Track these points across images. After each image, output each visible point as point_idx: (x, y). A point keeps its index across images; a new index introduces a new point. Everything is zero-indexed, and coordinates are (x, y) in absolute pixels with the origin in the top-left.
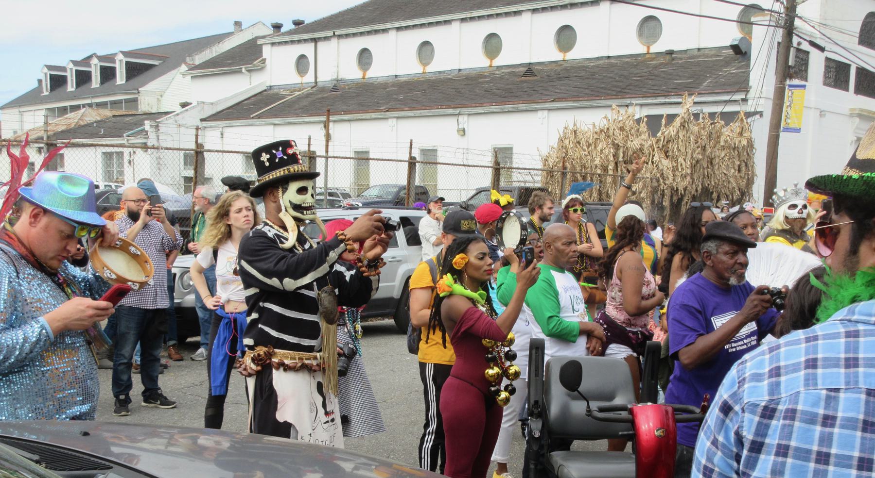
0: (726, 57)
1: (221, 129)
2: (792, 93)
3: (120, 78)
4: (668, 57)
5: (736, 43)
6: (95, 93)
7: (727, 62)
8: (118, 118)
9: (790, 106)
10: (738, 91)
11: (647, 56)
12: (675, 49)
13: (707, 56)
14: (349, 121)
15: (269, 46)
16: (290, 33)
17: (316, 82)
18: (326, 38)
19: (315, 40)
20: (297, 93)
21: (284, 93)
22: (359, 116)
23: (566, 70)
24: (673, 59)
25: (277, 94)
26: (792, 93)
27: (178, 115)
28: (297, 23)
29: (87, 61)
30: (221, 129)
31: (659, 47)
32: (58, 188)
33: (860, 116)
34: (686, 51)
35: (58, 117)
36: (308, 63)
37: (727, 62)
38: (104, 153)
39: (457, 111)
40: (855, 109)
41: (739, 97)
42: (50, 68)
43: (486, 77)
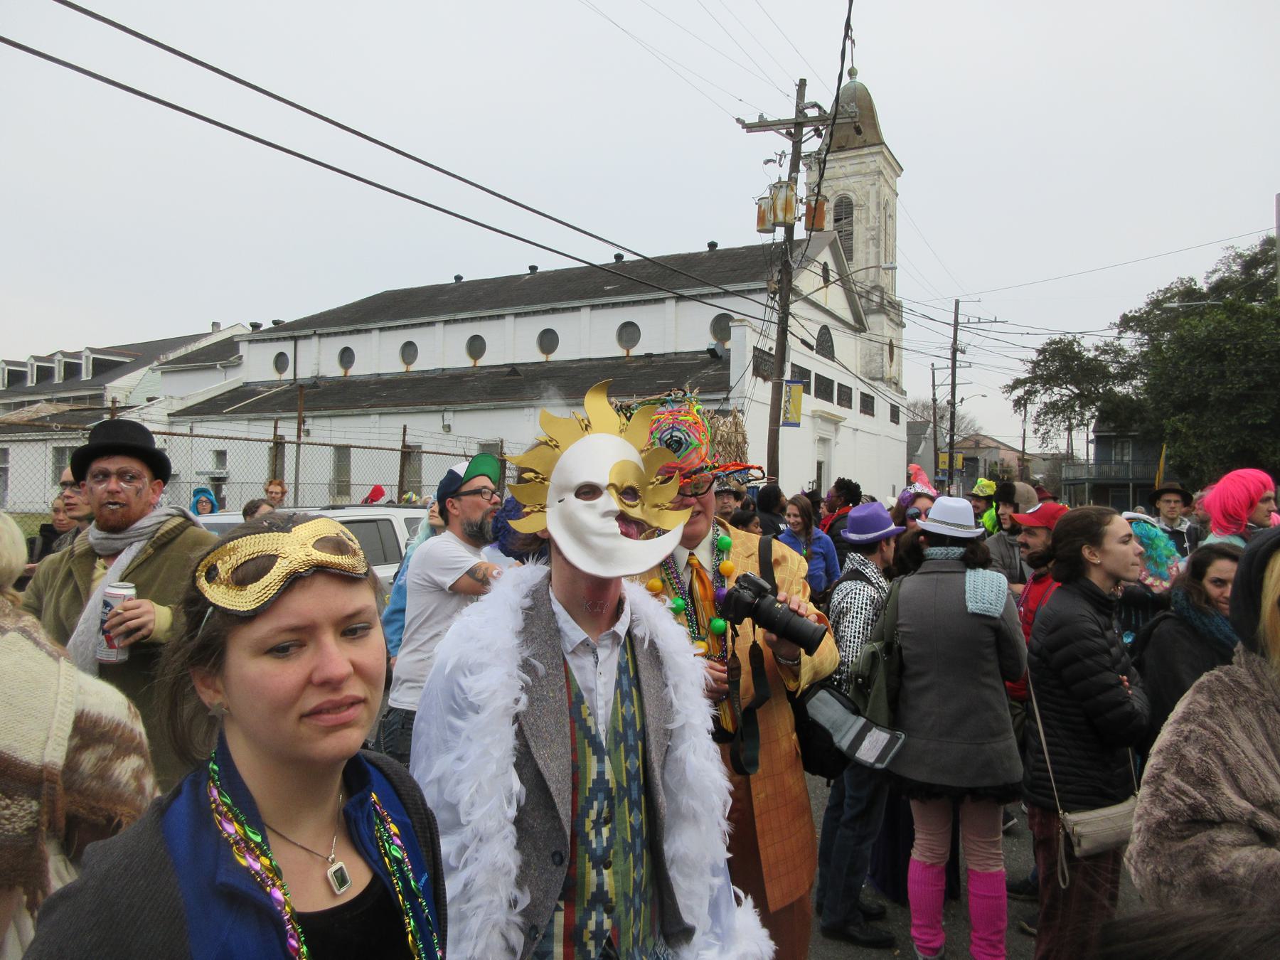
0: (702, 361)
1: (190, 424)
2: (790, 389)
3: (86, 375)
4: (647, 360)
5: (712, 347)
6: (58, 388)
7: (705, 365)
8: (76, 413)
9: (789, 401)
10: (719, 390)
11: (627, 359)
12: (655, 352)
13: (684, 359)
14: (329, 416)
15: (247, 343)
16: (269, 330)
17: (295, 379)
18: (307, 337)
19: (295, 339)
20: (275, 390)
21: (261, 389)
22: (340, 412)
23: (549, 370)
24: (652, 362)
25: (254, 390)
26: (790, 389)
27: (142, 409)
28: (275, 322)
29: (50, 358)
30: (190, 424)
31: (637, 351)
32: (728, 525)
33: (821, 417)
34: (663, 355)
35: (14, 410)
36: (287, 360)
37: (705, 365)
38: (55, 448)
39: (443, 408)
40: (816, 411)
41: (722, 396)
42: (8, 363)
43: (470, 376)
